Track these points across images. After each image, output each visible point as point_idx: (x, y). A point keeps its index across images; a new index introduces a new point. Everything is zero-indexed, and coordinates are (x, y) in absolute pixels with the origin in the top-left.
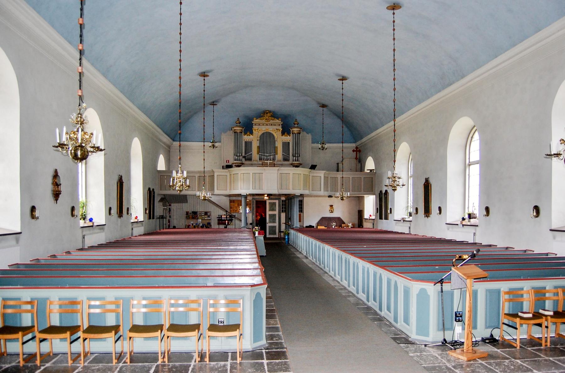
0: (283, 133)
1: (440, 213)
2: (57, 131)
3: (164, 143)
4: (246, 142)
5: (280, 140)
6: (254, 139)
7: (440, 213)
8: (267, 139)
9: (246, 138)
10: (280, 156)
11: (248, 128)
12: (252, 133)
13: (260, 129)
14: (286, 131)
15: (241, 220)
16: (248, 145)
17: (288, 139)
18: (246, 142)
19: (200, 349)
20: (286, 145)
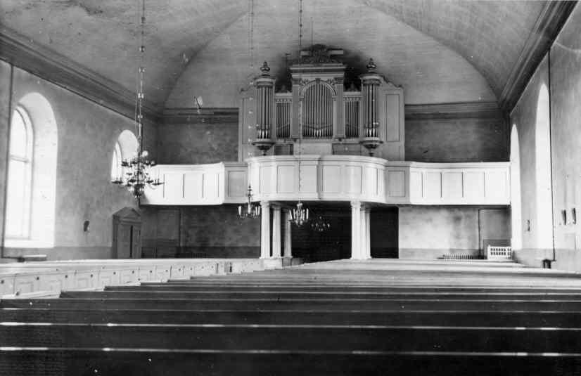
5: (341, 102)
12: (289, 88)
13: (305, 78)
16: (283, 108)
18: (279, 105)
19: (477, 248)
20: (354, 108)
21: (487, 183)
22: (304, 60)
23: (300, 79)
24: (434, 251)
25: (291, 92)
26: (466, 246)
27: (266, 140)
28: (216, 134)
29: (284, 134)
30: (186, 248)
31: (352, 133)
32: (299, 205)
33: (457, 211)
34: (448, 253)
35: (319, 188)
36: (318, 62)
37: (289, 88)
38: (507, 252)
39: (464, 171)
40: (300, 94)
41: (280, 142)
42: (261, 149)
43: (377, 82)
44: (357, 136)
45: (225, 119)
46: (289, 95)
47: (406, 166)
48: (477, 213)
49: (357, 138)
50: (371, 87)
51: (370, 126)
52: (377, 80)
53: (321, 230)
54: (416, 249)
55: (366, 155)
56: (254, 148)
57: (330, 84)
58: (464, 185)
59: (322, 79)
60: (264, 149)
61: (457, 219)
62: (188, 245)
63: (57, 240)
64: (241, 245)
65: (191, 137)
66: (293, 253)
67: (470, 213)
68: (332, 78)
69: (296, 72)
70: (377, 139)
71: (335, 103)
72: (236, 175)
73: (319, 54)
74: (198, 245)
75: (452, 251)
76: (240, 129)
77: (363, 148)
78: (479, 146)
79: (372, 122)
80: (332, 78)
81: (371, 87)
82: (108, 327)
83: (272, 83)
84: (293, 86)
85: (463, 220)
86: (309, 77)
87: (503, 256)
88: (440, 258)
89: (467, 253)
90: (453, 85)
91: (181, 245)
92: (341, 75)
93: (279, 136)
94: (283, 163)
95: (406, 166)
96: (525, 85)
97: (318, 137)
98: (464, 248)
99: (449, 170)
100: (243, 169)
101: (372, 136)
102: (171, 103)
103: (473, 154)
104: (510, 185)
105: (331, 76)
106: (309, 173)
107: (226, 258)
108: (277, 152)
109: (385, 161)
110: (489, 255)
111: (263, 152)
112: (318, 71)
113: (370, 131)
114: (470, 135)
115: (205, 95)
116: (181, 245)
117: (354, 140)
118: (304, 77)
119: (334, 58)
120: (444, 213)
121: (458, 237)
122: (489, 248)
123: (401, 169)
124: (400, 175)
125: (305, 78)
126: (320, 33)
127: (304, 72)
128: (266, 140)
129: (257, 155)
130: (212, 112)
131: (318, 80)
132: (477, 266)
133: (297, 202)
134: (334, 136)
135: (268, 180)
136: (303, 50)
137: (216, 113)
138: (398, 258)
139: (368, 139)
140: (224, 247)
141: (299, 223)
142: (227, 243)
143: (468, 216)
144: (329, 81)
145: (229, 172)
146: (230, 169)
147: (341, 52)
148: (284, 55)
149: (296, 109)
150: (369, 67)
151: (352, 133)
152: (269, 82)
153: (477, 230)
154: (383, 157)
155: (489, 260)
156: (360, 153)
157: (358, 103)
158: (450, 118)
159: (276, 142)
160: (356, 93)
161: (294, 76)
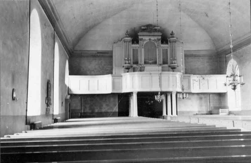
9: (135, 46)
10: (160, 60)
11: (135, 39)
12: (138, 43)
13: (145, 38)
16: (135, 52)
18: (133, 50)
19: (209, 110)
20: (165, 52)
21: (217, 83)
22: (144, 30)
23: (142, 39)
26: (205, 109)
27: (129, 65)
28: (104, 63)
29: (136, 63)
30: (84, 113)
31: (165, 62)
32: (159, 93)
33: (201, 95)
34: (197, 113)
36: (150, 32)
40: (142, 45)
41: (135, 66)
43: (175, 41)
44: (167, 63)
46: (137, 45)
47: (189, 77)
48: (209, 96)
49: (168, 64)
50: (127, 43)
52: (175, 40)
53: (150, 105)
55: (171, 71)
56: (123, 69)
57: (150, 41)
59: (152, 39)
60: (128, 69)
61: (201, 98)
62: (85, 111)
64: (109, 111)
65: (87, 64)
66: (140, 114)
67: (205, 96)
69: (140, 35)
70: (176, 65)
71: (157, 49)
72: (117, 80)
73: (149, 28)
74: (90, 111)
75: (199, 111)
77: (170, 69)
78: (209, 68)
80: (156, 39)
81: (173, 43)
82: (246, 155)
83: (130, 40)
84: (139, 42)
85: (203, 99)
86: (147, 38)
87: (226, 113)
89: (205, 113)
91: (82, 111)
92: (160, 37)
93: (134, 63)
94: (144, 75)
95: (189, 77)
97: (150, 64)
101: (174, 63)
102: (77, 48)
103: (206, 72)
104: (152, 83)
105: (156, 38)
106: (156, 78)
107: (152, 117)
108: (134, 71)
111: (127, 70)
112: (149, 36)
115: (96, 43)
116: (82, 111)
117: (166, 65)
118: (144, 38)
119: (156, 30)
120: (196, 96)
121: (201, 106)
124: (187, 80)
125: (145, 38)
126: (151, 21)
127: (144, 36)
128: (129, 65)
129: (125, 72)
130: (96, 52)
131: (150, 39)
133: (158, 92)
134: (157, 64)
135: (132, 83)
137: (98, 53)
139: (172, 65)
141: (160, 101)
142: (103, 110)
143: (205, 97)
144: (155, 40)
145: (114, 79)
146: (114, 77)
147: (159, 28)
149: (141, 51)
151: (165, 62)
152: (129, 40)
153: (209, 103)
156: (169, 71)
157: (167, 50)
158: (197, 56)
159: (133, 66)
160: (167, 45)
161: (140, 37)
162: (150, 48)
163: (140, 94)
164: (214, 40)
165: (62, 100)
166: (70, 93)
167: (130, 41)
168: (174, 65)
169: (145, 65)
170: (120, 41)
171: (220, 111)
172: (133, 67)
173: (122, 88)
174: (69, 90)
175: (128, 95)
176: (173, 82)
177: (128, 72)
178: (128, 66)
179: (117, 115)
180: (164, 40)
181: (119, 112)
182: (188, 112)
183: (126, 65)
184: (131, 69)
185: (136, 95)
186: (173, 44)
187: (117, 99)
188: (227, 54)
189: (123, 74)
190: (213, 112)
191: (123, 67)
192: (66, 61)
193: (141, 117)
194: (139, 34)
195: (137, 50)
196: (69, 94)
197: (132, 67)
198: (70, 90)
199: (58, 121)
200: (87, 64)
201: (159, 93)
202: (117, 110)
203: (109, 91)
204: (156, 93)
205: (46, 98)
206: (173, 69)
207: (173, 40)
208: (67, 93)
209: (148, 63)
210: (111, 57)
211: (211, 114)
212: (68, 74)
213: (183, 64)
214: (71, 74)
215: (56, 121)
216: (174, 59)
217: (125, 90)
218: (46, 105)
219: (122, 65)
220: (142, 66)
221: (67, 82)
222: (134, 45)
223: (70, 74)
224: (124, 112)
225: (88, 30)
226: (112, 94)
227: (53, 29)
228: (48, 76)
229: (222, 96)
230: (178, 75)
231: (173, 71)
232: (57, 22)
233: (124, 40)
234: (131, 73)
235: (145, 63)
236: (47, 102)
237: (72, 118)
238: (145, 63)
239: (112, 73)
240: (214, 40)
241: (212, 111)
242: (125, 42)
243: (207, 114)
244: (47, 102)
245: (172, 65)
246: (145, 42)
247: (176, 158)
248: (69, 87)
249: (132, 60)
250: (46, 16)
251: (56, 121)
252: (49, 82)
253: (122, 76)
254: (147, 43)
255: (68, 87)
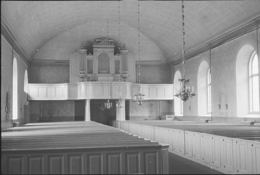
0: (115, 54)
1: (220, 108)
2: (105, 104)
3: (86, 89)
4: (88, 61)
5: (113, 59)
6: (94, 58)
7: (220, 108)
8: (103, 58)
9: (90, 57)
10: (112, 69)
11: (90, 50)
12: (92, 53)
13: (98, 51)
14: (117, 51)
15: (14, 127)
16: (90, 62)
17: (118, 57)
18: (88, 61)
19: (159, 116)
20: (117, 63)
23: (97, 51)
24: (143, 117)
25: (93, 55)
28: (61, 72)
29: (91, 72)
30: (43, 117)
32: (108, 101)
33: (152, 103)
35: (111, 95)
37: (119, 53)
38: (173, 117)
39: (157, 87)
41: (89, 75)
42: (82, 78)
44: (118, 73)
45: (65, 65)
49: (120, 74)
51: (125, 70)
53: (104, 112)
54: (137, 116)
58: (253, 94)
59: (105, 51)
63: (14, 120)
66: (92, 120)
68: (109, 51)
75: (149, 117)
76: (70, 70)
79: (125, 69)
81: (125, 55)
84: (94, 53)
87: (172, 118)
88: (145, 120)
90: (151, 54)
93: (89, 73)
96: (194, 56)
98: (154, 116)
99: (152, 87)
100: (75, 86)
105: (110, 50)
109: (132, 83)
110: (167, 118)
113: (125, 72)
114: (156, 74)
115: (55, 53)
116: (41, 116)
117: (118, 75)
121: (151, 112)
122: (167, 115)
123: (29, 88)
128: (84, 75)
130: (54, 61)
132: (207, 124)
133: (107, 100)
134: (110, 74)
135: (85, 92)
136: (97, 39)
137: (56, 62)
138: (129, 120)
140: (60, 117)
144: (108, 52)
147: (112, 41)
148: (89, 40)
150: (124, 48)
151: (117, 72)
154: (129, 82)
155: (167, 120)
159: (89, 76)
162: (103, 58)
163: (92, 101)
164: (164, 52)
165: (21, 106)
166: (29, 99)
167: (85, 52)
168: (125, 75)
169: (99, 75)
170: (76, 52)
171: (167, 117)
172: (87, 77)
173: (77, 96)
174: (28, 96)
175: (83, 102)
176: (124, 91)
177: (83, 81)
178: (83, 76)
179: (74, 120)
180: (117, 51)
181: (75, 116)
182: (140, 117)
183: (81, 74)
184: (85, 79)
185: (89, 102)
186: (125, 56)
187: (74, 105)
188: (175, 65)
189: (78, 83)
190: (162, 118)
191: (79, 76)
192: (25, 71)
193: (93, 122)
194: (93, 46)
195: (92, 61)
196: (28, 101)
197: (86, 76)
198: (29, 96)
199: (17, 125)
200: (44, 73)
201: (108, 101)
202: (74, 115)
203: (65, 98)
204: (106, 101)
205: (6, 107)
206: (124, 78)
207: (125, 52)
208: (26, 100)
209: (101, 73)
210: (68, 66)
211: (160, 119)
212: (27, 82)
213: (197, 48)
214: (30, 82)
215: (14, 125)
216: (125, 70)
217: (80, 97)
218: (6, 112)
219: (78, 75)
220: (96, 75)
221: (26, 90)
222: (88, 56)
223: (29, 83)
224: (80, 117)
225: (47, 40)
226: (68, 100)
227: (12, 48)
228: (7, 89)
229: (170, 103)
230: (128, 85)
231: (125, 81)
232: (15, 41)
233: (80, 52)
234: (86, 82)
235: (99, 73)
236: (6, 110)
237: (30, 123)
238: (99, 73)
239: (67, 81)
240: (164, 52)
241: (162, 116)
242: (80, 53)
243: (156, 119)
244: (6, 110)
245: (124, 75)
246: (98, 54)
247: (10, 128)
248: (29, 94)
249: (87, 70)
250: (5, 39)
251: (15, 125)
252: (8, 93)
253: (77, 85)
254: (100, 55)
255: (28, 94)
